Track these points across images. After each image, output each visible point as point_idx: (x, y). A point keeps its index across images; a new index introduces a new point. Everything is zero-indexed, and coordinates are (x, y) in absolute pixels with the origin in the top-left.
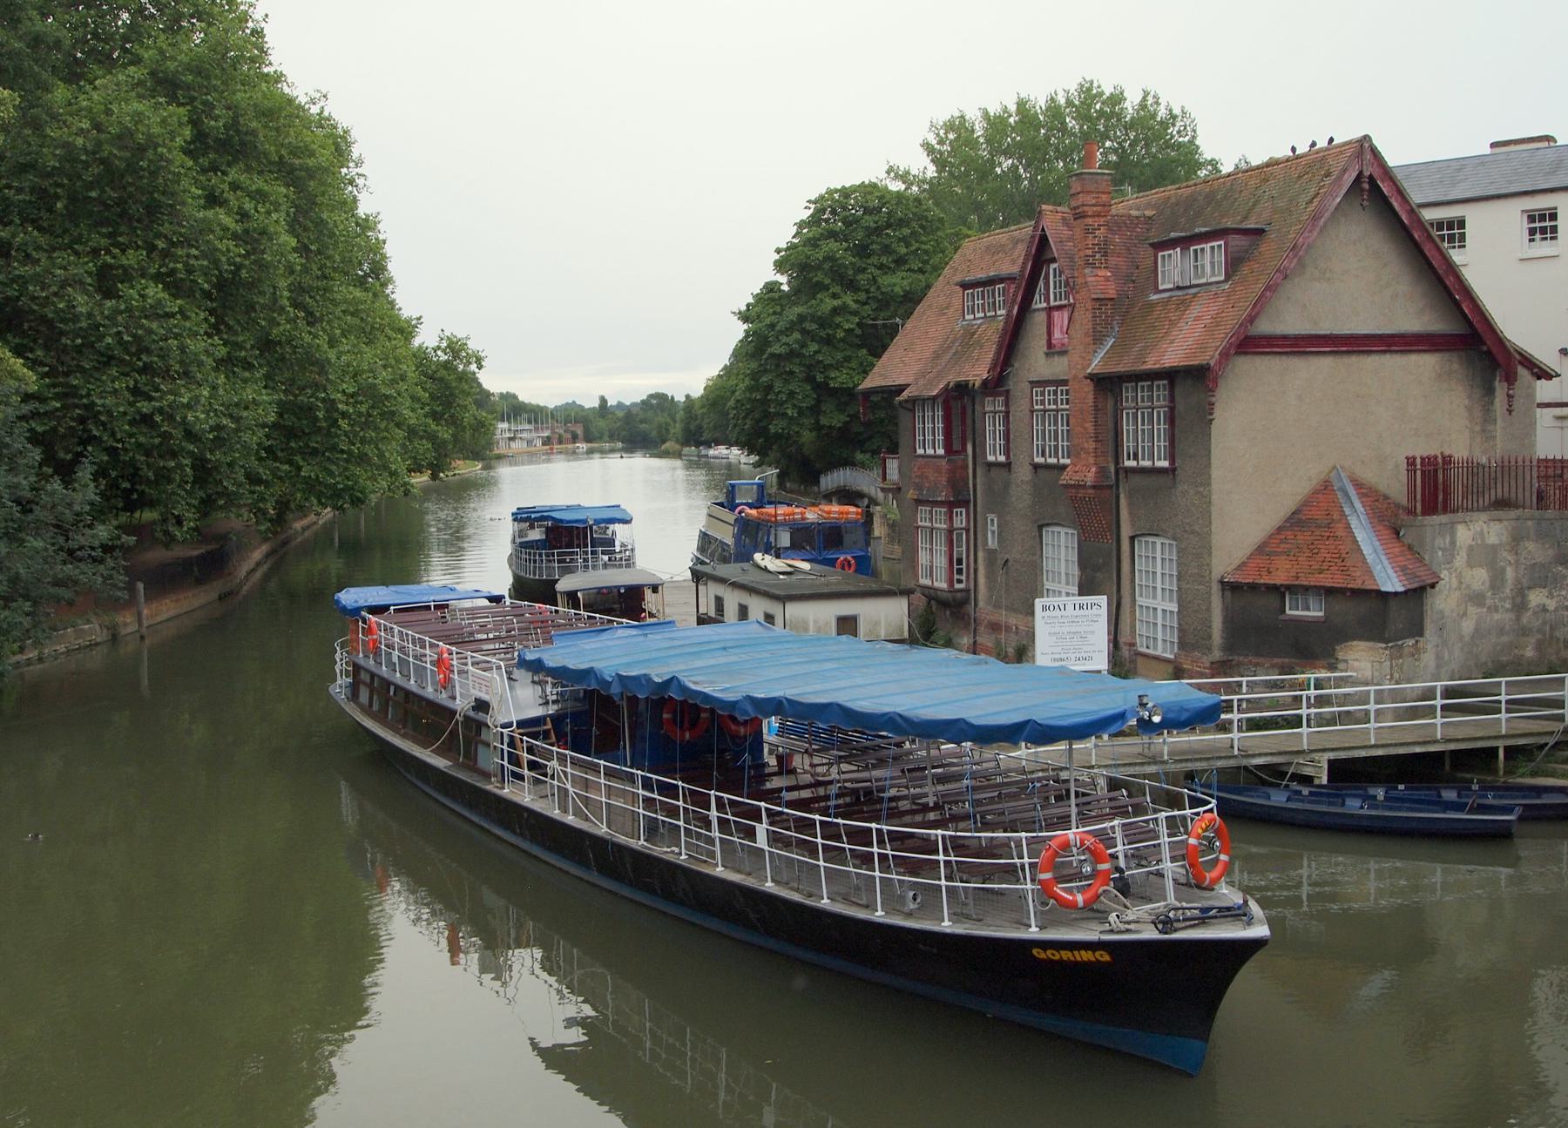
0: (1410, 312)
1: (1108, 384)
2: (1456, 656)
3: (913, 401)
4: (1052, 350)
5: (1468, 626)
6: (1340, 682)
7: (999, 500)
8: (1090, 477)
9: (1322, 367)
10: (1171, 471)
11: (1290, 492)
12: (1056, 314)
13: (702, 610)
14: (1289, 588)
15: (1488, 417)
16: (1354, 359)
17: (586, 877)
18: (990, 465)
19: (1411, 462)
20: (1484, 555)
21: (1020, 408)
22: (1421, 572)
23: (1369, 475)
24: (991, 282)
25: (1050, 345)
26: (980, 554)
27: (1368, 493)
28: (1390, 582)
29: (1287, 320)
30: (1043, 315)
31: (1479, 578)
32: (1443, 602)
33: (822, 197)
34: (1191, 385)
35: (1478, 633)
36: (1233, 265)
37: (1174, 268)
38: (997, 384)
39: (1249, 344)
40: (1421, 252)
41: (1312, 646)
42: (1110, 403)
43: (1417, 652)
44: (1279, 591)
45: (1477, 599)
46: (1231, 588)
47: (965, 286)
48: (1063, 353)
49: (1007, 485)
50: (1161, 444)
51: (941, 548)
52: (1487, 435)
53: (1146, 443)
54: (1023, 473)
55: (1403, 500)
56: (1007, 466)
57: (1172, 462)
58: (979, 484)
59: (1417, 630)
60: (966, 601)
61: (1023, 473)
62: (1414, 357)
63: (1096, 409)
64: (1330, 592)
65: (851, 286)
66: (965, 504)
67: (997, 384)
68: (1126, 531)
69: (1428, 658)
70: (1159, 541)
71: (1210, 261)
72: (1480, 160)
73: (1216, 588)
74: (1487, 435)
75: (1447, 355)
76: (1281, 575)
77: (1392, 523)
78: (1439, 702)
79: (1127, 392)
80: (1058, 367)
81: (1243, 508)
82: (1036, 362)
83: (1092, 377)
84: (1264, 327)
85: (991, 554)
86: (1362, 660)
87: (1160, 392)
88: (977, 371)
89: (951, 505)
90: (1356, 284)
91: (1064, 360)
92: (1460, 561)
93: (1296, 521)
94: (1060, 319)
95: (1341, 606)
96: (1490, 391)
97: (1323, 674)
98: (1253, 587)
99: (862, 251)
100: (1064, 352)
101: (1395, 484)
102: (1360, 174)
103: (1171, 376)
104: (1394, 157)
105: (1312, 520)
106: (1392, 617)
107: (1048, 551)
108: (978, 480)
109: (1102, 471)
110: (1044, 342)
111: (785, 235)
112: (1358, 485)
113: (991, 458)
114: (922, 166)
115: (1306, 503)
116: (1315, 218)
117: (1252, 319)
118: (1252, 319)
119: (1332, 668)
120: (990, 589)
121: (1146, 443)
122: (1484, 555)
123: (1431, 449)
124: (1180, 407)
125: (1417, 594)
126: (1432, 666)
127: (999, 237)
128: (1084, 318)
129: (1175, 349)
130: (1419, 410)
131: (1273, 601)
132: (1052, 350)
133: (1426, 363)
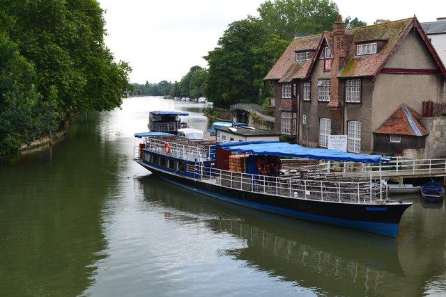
0: (424, 64)
1: (343, 81)
2: (432, 154)
3: (282, 83)
4: (325, 70)
5: (435, 146)
6: (405, 159)
7: (307, 111)
8: (336, 104)
9: (400, 78)
10: (361, 103)
11: (392, 109)
12: (327, 61)
13: (278, 140)
14: (391, 134)
15: (442, 92)
16: (409, 75)
17: (241, 203)
18: (305, 101)
19: (423, 103)
20: (439, 128)
21: (314, 87)
22: (426, 131)
23: (411, 106)
24: (305, 51)
25: (325, 69)
26: (301, 126)
27: (412, 111)
28: (418, 133)
29: (393, 65)
30: (323, 61)
31: (438, 134)
32: (430, 140)
33: (233, 23)
34: (367, 82)
35: (437, 148)
36: (379, 49)
37: (361, 50)
38: (308, 79)
39: (383, 70)
40: (428, 48)
41: (398, 150)
42: (343, 86)
43: (423, 152)
44: (388, 135)
45: (437, 139)
46: (375, 134)
47: (296, 52)
48: (329, 71)
49: (309, 107)
50: (359, 96)
51: (289, 124)
52: (441, 97)
53: (353, 96)
54: (315, 103)
55: (421, 113)
56: (310, 102)
57: (310, 97)
58: (300, 106)
59: (423, 147)
60: (296, 138)
61: (315, 103)
62: (424, 75)
63: (339, 87)
64: (403, 136)
65: (241, 50)
66: (296, 112)
67: (308, 79)
68: (346, 119)
69: (426, 154)
70: (355, 122)
71: (372, 48)
72: (434, 24)
73: (372, 134)
74: (441, 97)
75: (432, 76)
76: (389, 131)
77: (418, 120)
78: (430, 164)
79: (348, 84)
80: (327, 75)
81: (379, 116)
82: (320, 73)
83: (338, 78)
84: (388, 66)
85: (304, 126)
86: (410, 154)
87: (358, 84)
88: (302, 74)
89: (292, 112)
90: (411, 56)
91: (329, 73)
92: (434, 129)
93: (393, 118)
94: (328, 63)
95: (404, 140)
96: (442, 85)
97: (400, 157)
98: (382, 134)
99: (245, 40)
100: (329, 68)
101: (418, 109)
102: (413, 27)
103: (362, 78)
104: (421, 21)
105: (396, 117)
106: (418, 143)
107: (321, 125)
108: (443, 20)
109: (340, 103)
110: (323, 68)
111: (222, 34)
112: (409, 109)
113: (305, 99)
114: (257, 15)
115: (395, 113)
116: (401, 38)
117: (384, 64)
118: (384, 64)
119: (402, 155)
120: (304, 135)
121: (353, 96)
122: (439, 128)
123: (427, 100)
124: (364, 86)
125: (424, 137)
126: (427, 157)
127: (313, 36)
128: (336, 62)
129: (362, 70)
130: (424, 89)
131: (387, 138)
132: (325, 70)
133: (427, 77)
